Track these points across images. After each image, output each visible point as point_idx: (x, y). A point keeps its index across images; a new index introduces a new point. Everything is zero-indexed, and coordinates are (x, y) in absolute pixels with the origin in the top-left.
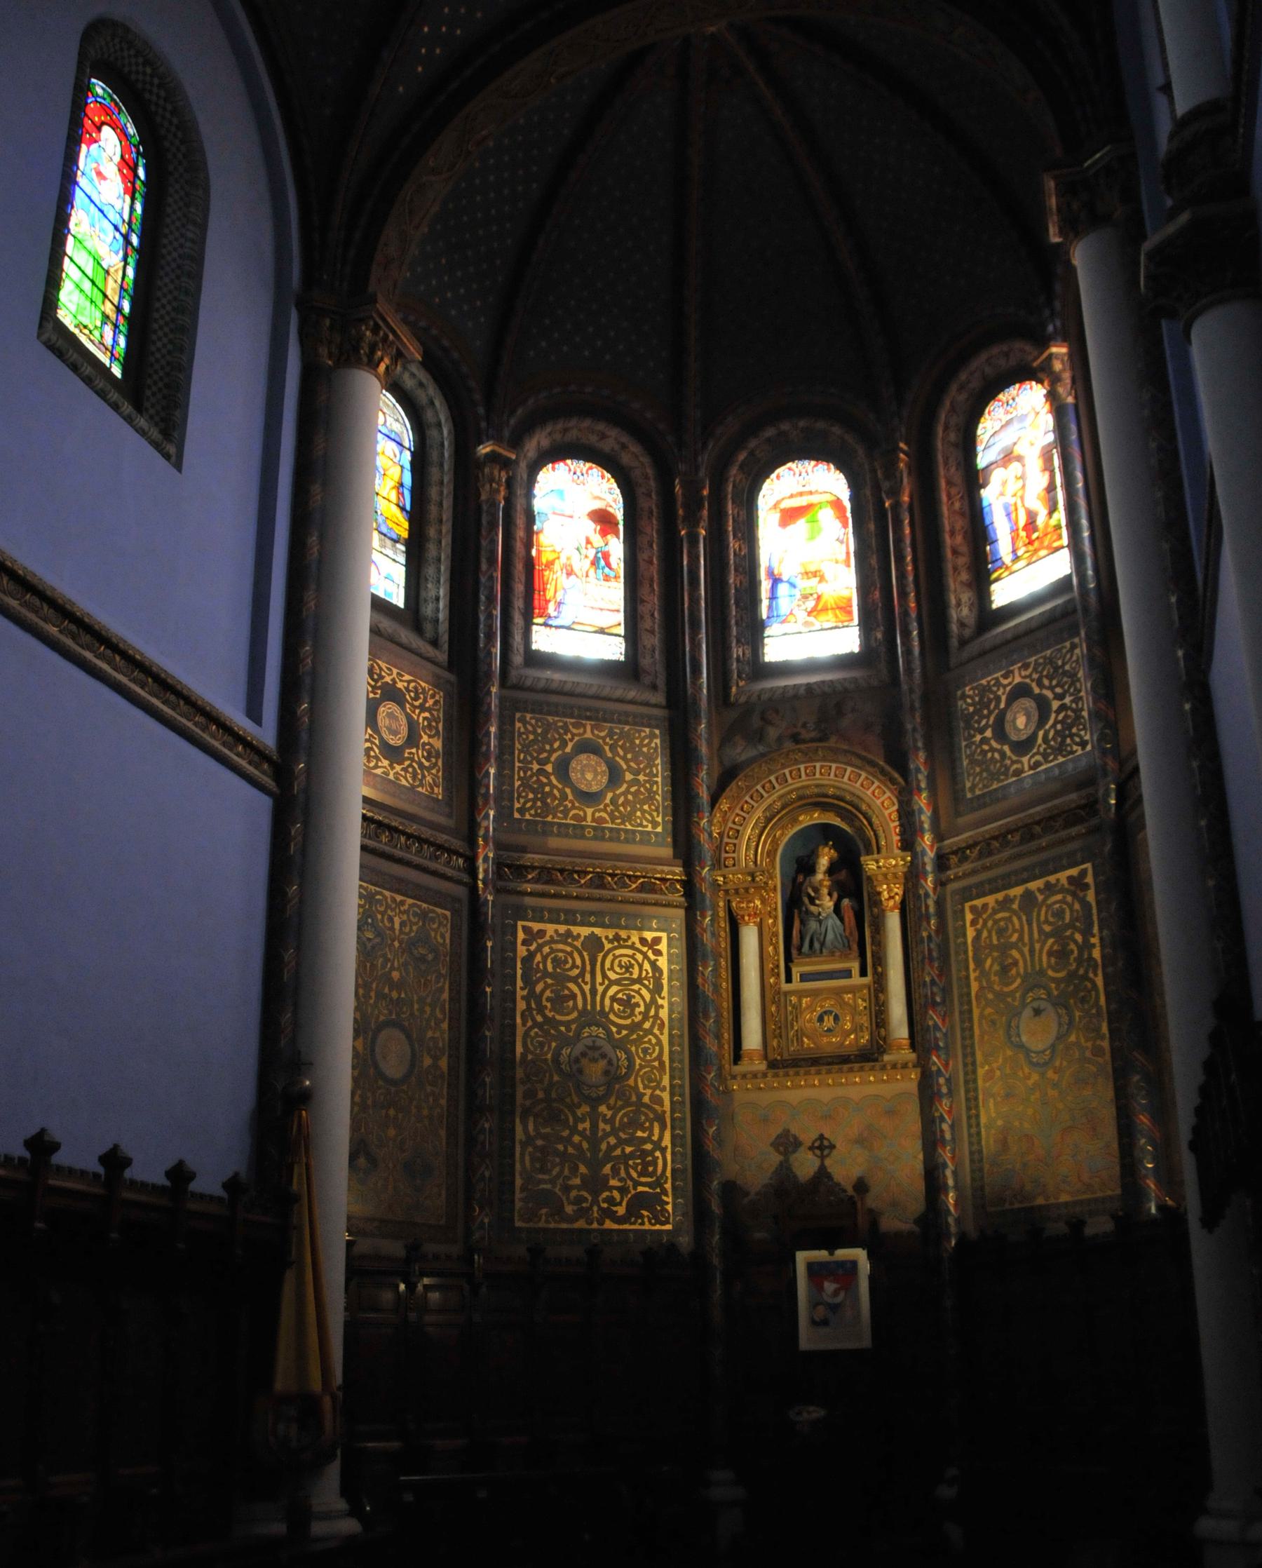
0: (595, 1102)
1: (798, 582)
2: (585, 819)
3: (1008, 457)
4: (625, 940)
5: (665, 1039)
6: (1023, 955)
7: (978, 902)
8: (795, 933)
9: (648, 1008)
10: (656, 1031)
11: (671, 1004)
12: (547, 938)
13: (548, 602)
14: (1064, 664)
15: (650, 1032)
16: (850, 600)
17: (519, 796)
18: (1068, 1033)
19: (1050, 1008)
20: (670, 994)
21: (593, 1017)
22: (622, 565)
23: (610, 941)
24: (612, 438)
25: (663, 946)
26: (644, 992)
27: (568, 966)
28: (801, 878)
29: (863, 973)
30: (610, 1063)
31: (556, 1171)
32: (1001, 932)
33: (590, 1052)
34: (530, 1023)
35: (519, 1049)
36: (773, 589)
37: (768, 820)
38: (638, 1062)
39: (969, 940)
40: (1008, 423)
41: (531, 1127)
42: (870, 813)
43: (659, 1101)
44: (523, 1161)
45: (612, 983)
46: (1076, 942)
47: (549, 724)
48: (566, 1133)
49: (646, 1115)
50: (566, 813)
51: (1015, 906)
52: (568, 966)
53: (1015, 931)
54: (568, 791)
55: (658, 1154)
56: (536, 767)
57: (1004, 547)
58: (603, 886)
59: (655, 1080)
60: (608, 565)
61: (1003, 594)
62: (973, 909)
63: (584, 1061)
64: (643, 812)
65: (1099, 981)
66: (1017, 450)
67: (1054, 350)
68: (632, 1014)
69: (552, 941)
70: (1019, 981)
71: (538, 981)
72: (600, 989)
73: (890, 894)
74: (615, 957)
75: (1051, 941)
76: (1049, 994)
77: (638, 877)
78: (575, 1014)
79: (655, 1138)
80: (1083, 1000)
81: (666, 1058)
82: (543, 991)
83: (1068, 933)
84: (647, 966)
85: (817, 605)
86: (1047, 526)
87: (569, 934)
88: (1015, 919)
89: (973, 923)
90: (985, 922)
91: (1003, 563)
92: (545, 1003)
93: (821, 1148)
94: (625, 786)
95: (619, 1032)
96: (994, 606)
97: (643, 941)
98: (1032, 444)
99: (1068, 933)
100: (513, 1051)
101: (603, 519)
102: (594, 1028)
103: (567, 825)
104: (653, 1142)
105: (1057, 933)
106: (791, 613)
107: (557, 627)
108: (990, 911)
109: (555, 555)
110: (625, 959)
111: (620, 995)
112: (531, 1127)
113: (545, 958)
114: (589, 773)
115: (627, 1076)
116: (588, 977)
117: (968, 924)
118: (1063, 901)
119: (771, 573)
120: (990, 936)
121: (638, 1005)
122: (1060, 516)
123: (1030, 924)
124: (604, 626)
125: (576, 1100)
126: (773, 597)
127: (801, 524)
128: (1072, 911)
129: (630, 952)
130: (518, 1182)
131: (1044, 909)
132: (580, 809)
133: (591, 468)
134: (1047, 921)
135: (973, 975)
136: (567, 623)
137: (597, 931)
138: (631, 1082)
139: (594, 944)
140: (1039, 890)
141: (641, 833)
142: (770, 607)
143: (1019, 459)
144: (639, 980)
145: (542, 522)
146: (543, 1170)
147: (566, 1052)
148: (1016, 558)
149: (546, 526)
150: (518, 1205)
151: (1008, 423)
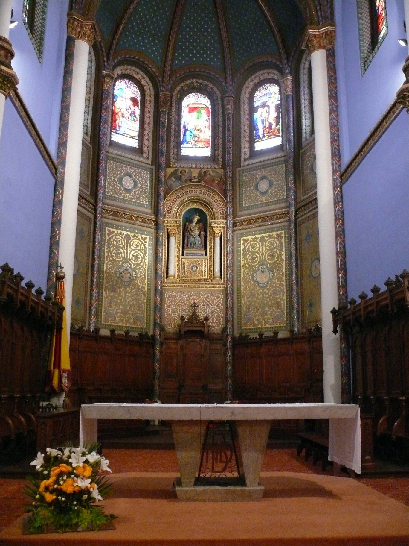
0: (126, 287)
1: (193, 131)
2: (126, 197)
3: (264, 105)
4: (137, 237)
5: (146, 269)
6: (259, 254)
7: (246, 238)
8: (186, 241)
9: (142, 259)
10: (144, 266)
11: (149, 259)
12: (115, 234)
13: (117, 125)
14: (279, 171)
15: (142, 266)
16: (209, 140)
17: (108, 187)
18: (272, 279)
19: (267, 271)
20: (149, 255)
21: (127, 260)
22: (139, 117)
23: (133, 237)
24: (140, 75)
25: (147, 240)
26: (141, 254)
27: (120, 243)
28: (187, 224)
29: (206, 255)
30: (131, 275)
31: (114, 308)
32: (252, 248)
33: (125, 271)
34: (109, 260)
35: (105, 268)
36: (185, 133)
37: (181, 205)
38: (139, 275)
39: (242, 249)
40: (265, 95)
41: (107, 293)
42: (213, 207)
43: (144, 288)
44: (105, 303)
45: (133, 250)
46: (277, 253)
47: (117, 165)
48: (117, 296)
49: (140, 292)
50: (121, 194)
51: (258, 240)
52: (120, 243)
53: (257, 247)
54: (122, 187)
55: (282, 302)
56: (113, 179)
57: (260, 133)
58: (131, 219)
59: (143, 282)
60: (135, 116)
61: (259, 146)
62: (244, 240)
63: (123, 274)
64: (143, 197)
65: (284, 265)
66: (268, 104)
67: (288, 78)
68: (138, 260)
69: (116, 235)
70: (257, 262)
71: (247, 254)
72: (129, 252)
73: (218, 232)
74: (134, 242)
75: (269, 252)
76: (267, 267)
77: (141, 218)
78: (122, 259)
79: (142, 299)
80: (278, 270)
81: (146, 275)
82: (113, 251)
83: (275, 250)
84: (142, 246)
85: (198, 140)
86: (275, 128)
87: (121, 233)
88: (257, 244)
89: (244, 244)
90: (248, 244)
91: (260, 137)
92: (113, 254)
93: (194, 306)
94: (138, 188)
95: (134, 266)
96: (255, 150)
97: (142, 238)
98: (273, 103)
99: (275, 250)
100: (103, 269)
101: (134, 100)
102: (127, 264)
103: (121, 199)
104: (281, 299)
105: (271, 250)
106: (190, 141)
107: (119, 134)
108: (249, 241)
109: (120, 110)
110: (136, 243)
111: (134, 254)
112: (107, 293)
113: (114, 240)
114: (128, 183)
115: (135, 279)
116: (126, 247)
117: (242, 244)
118: (274, 241)
119: (184, 127)
120: (249, 248)
121: (139, 258)
122: (279, 126)
123: (262, 246)
124: (133, 136)
125: (120, 285)
126: (185, 135)
127: (195, 114)
128: (276, 244)
129: (138, 241)
130: (103, 310)
131: (267, 242)
132: (125, 194)
133: (131, 83)
134: (268, 246)
135: (242, 259)
136: (122, 133)
137: (129, 233)
138: (136, 281)
139: (128, 237)
140: (266, 236)
141: (142, 204)
142: (183, 138)
143: (268, 106)
144: (140, 250)
145: (116, 99)
146: (110, 306)
147: (118, 270)
148: (264, 136)
149: (117, 100)
150: (103, 317)
151: (265, 95)
